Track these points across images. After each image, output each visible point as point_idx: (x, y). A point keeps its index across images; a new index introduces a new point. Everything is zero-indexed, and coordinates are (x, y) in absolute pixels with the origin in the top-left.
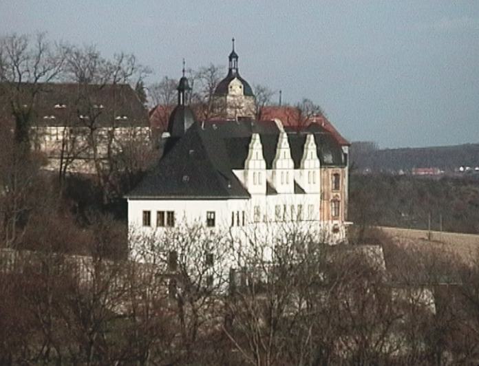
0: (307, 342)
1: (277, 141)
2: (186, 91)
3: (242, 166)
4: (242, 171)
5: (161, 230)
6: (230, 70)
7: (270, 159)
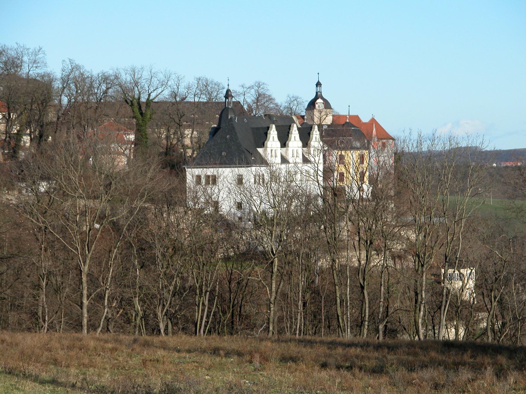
0: (161, 286)
1: (290, 129)
2: (230, 99)
3: (263, 145)
6: (317, 93)
7: (284, 141)
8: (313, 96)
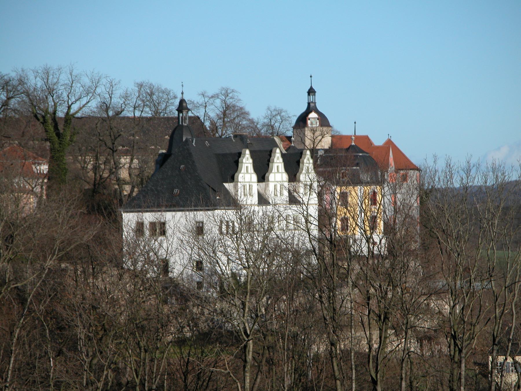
3: (232, 179)
4: (232, 184)
6: (309, 104)
7: (262, 172)
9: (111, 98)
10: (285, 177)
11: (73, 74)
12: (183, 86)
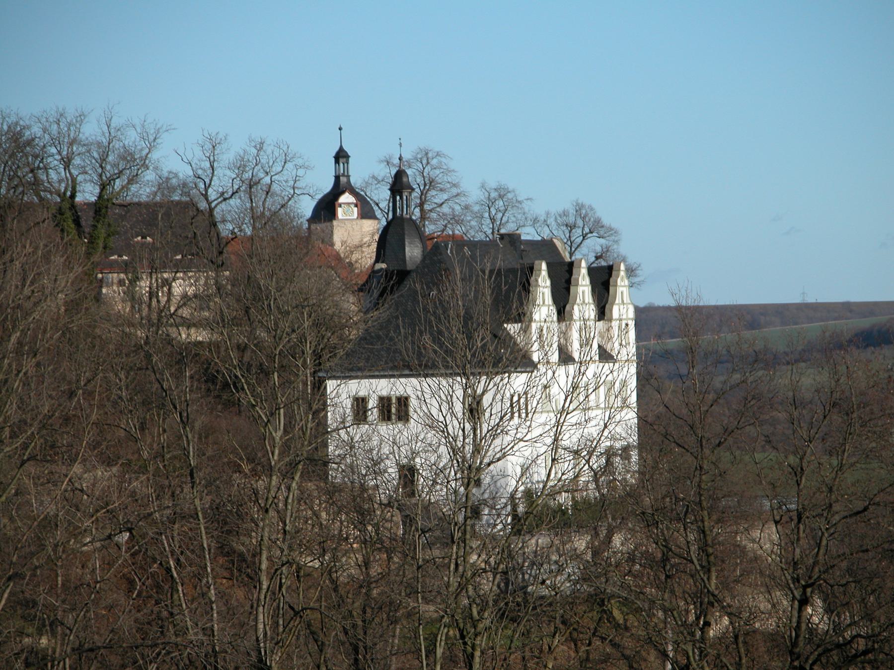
4: (517, 326)
5: (384, 429)
6: (337, 178)
8: (327, 185)
9: (212, 167)
10: (553, 309)
11: (113, 125)
12: (401, 145)
